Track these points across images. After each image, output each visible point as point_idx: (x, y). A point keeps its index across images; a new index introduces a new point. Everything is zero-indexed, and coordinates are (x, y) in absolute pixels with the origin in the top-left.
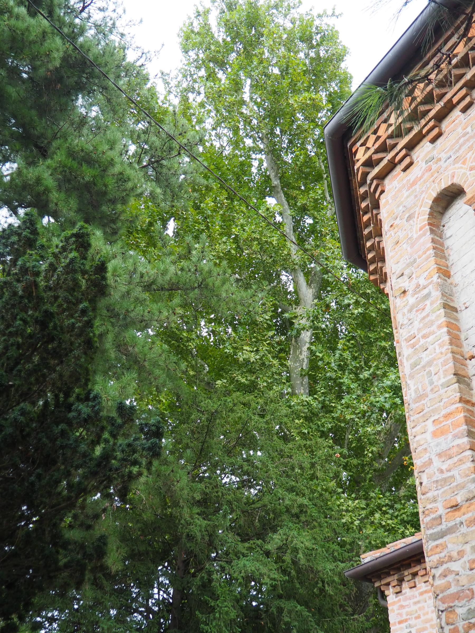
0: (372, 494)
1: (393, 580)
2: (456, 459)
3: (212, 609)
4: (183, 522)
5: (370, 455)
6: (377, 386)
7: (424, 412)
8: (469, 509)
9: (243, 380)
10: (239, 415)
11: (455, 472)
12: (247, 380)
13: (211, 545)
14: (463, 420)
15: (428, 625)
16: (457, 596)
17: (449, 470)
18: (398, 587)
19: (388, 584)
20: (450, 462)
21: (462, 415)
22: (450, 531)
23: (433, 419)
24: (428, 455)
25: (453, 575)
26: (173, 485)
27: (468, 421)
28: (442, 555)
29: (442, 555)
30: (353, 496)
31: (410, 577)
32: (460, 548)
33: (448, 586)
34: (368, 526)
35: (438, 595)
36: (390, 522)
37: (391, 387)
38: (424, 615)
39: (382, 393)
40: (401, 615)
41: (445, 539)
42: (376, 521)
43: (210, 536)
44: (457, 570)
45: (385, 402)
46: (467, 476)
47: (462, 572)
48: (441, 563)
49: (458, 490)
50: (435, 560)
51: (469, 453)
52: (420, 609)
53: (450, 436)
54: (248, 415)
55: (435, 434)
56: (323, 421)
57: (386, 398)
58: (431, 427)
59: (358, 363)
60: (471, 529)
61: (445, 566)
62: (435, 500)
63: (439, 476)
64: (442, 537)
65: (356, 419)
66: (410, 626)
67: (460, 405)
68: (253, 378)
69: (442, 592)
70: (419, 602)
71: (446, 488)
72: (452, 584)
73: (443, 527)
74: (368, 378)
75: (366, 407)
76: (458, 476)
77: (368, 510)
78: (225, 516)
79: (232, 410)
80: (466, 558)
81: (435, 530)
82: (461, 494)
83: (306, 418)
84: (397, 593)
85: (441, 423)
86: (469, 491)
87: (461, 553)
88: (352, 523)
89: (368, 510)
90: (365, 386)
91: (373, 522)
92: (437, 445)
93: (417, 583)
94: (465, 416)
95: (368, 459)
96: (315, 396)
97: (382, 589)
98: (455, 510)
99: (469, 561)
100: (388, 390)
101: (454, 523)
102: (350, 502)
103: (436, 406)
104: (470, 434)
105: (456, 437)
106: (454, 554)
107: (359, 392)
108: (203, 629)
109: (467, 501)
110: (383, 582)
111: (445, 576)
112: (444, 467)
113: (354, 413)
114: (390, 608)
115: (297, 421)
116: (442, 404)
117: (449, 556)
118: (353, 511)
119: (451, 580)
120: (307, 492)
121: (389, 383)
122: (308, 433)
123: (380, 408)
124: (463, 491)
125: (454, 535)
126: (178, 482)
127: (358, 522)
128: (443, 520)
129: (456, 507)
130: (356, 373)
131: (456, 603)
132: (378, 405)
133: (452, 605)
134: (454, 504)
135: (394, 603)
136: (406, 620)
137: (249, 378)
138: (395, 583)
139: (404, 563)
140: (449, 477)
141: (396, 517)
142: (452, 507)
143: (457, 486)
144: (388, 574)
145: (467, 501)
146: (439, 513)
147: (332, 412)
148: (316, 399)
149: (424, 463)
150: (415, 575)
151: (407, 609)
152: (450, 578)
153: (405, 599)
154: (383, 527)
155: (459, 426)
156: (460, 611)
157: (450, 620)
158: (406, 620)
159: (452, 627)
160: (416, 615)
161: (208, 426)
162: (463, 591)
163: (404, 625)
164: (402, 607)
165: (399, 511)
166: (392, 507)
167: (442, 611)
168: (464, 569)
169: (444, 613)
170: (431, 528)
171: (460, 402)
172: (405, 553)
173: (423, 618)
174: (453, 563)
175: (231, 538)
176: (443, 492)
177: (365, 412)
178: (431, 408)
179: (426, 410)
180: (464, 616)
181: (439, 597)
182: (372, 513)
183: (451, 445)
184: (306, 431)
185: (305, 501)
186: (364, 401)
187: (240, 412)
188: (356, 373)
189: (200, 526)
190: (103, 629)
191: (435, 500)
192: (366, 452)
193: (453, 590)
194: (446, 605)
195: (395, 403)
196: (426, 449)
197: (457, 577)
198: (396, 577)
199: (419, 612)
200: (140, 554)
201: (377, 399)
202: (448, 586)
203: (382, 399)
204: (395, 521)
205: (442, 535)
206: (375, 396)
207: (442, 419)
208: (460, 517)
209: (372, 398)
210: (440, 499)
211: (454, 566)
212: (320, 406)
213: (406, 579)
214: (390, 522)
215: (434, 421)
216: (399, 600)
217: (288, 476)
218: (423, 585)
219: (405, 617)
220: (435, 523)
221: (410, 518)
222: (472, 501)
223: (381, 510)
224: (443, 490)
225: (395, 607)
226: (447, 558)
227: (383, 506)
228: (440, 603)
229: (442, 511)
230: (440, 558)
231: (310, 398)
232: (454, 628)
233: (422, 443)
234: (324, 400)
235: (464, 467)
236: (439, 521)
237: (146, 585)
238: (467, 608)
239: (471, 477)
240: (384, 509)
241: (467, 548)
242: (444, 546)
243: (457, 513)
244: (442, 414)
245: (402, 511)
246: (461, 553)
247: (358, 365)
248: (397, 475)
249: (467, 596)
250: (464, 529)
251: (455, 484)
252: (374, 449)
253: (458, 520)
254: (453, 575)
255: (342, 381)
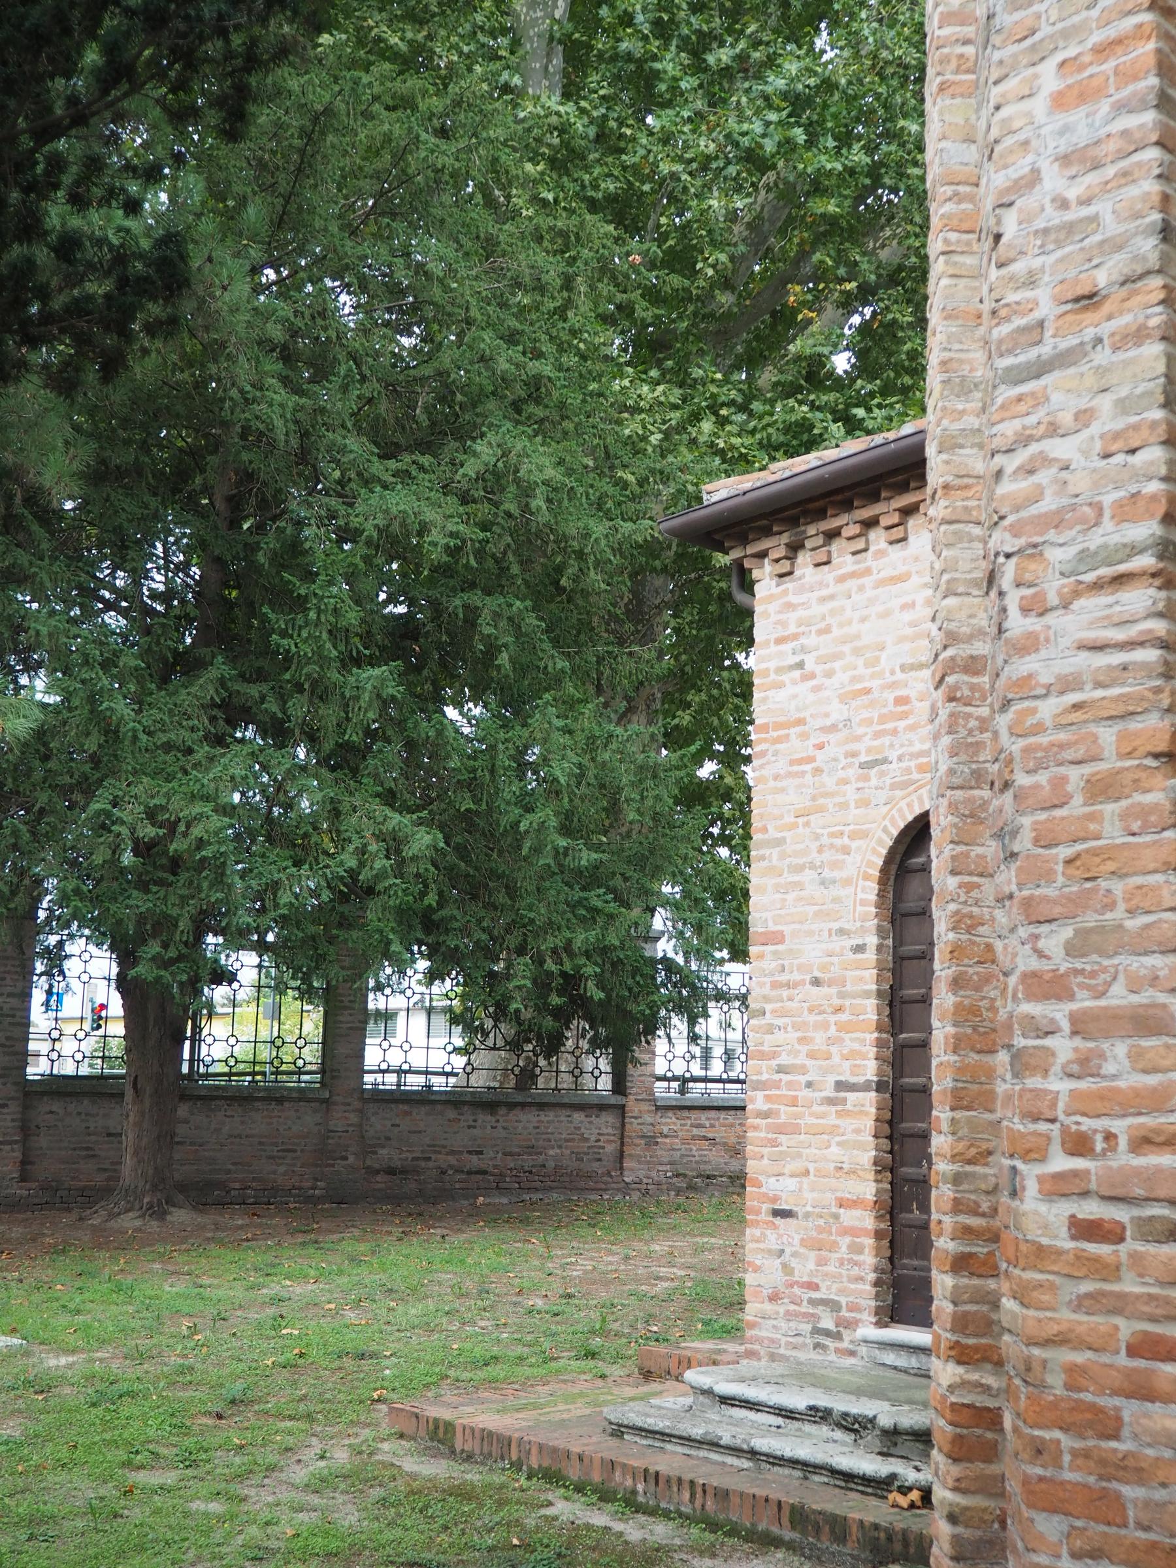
0: (697, 373)
1: (777, 545)
2: (1110, 171)
3: (301, 604)
4: (234, 393)
5: (710, 272)
6: (748, 91)
7: (1038, 36)
8: (1127, 304)
9: (394, 40)
10: (386, 127)
11: (1103, 208)
12: (402, 39)
13: (304, 458)
14: (1151, 61)
15: (846, 648)
16: (1056, 520)
17: (1086, 201)
18: (787, 563)
19: (762, 555)
20: (1093, 178)
21: (1151, 45)
22: (1063, 360)
23: (1059, 57)
24: (1030, 158)
25: (1054, 470)
26: (213, 297)
27: (1164, 68)
28: (1032, 420)
29: (1032, 420)
30: (654, 373)
31: (820, 540)
32: (1083, 403)
33: (1036, 496)
34: (683, 449)
35: (1002, 518)
36: (736, 441)
37: (785, 95)
38: (841, 626)
39: (758, 112)
40: (783, 624)
41: (1046, 380)
42: (702, 439)
43: (304, 435)
44: (1065, 456)
45: (764, 136)
46: (1138, 216)
47: (1078, 461)
48: (1025, 440)
49: (1103, 253)
50: (1010, 433)
51: (1154, 153)
52: (833, 613)
53: (1105, 107)
54: (410, 129)
55: (1059, 101)
56: (597, 171)
57: (768, 124)
58: (1049, 78)
59: (708, 22)
60: (1121, 356)
61: (1034, 448)
62: (1031, 281)
63: (1054, 217)
64: (1038, 376)
65: (685, 177)
66: (804, 650)
67: (1147, 17)
68: (420, 37)
69: (1017, 509)
70: (832, 597)
71: (1068, 249)
72: (1048, 492)
73: (1046, 350)
74: (728, 68)
75: (712, 146)
76: (1108, 218)
77: (687, 409)
78: (345, 389)
79: (368, 116)
80: (1095, 429)
81: (1022, 358)
82: (1110, 263)
83: (552, 162)
84: (781, 576)
85: (1082, 68)
86: (1135, 258)
87: (1084, 417)
88: (644, 439)
89: (687, 409)
90: (717, 87)
91: (693, 441)
92: (1062, 132)
93: (834, 555)
94: (1159, 51)
95: (702, 283)
96: (583, 104)
97: (747, 565)
98: (1086, 308)
99: (1102, 437)
100: (776, 101)
101: (1076, 341)
102: (646, 388)
103: (1076, 19)
104: (1164, 102)
105: (1122, 108)
106: (1066, 419)
107: (700, 104)
108: (278, 646)
109: (1123, 283)
110: (750, 550)
111: (1031, 472)
112: (1072, 194)
113: (680, 159)
114: (758, 609)
115: (529, 167)
116: (1095, 13)
117: (1051, 424)
118: (650, 410)
119: (1045, 482)
120: (547, 347)
121: (781, 83)
122: (556, 200)
123: (749, 151)
124: (1117, 257)
125: (1072, 370)
126: (225, 288)
127: (659, 436)
128: (1048, 334)
129: (1089, 300)
130: (698, 47)
131: (1051, 535)
132: (745, 142)
133: (1038, 539)
134: (1086, 290)
135: (770, 598)
136: (795, 637)
137: (409, 35)
138: (781, 552)
139: (811, 506)
140: (1081, 220)
141: (753, 432)
142: (1077, 300)
143: (1103, 242)
144: (767, 532)
145: (1123, 283)
146: (1037, 315)
147: (622, 151)
148: (583, 111)
149: (1016, 181)
150: (832, 535)
151: (801, 613)
152: (1044, 477)
153: (800, 591)
154: (722, 453)
155: (1136, 78)
156: (1055, 555)
157: (1028, 577)
158: (795, 637)
159: (1028, 592)
160: (822, 625)
161: (302, 152)
162: (1073, 508)
163: (787, 647)
164: (790, 606)
165: (760, 418)
166: (744, 408)
167: (1008, 556)
168: (1086, 454)
169: (1014, 560)
170: (1010, 352)
171: (1150, 8)
172: (820, 481)
173: (836, 632)
174: (1057, 441)
175: (356, 445)
176: (1061, 260)
177: (709, 158)
178: (1059, 26)
179: (1045, 30)
180: (1066, 568)
181: (1006, 522)
182: (696, 417)
183: (1103, 132)
184: (550, 197)
185: (546, 368)
186: (710, 130)
187: (390, 124)
188: (698, 47)
189: (281, 405)
190: (38, 633)
191: (1031, 281)
192: (699, 266)
193: (1048, 504)
194: (1022, 542)
195: (788, 141)
196: (1026, 143)
197: (1064, 474)
198: (785, 538)
199: (829, 620)
200: (120, 473)
201: (745, 127)
202: (1036, 496)
203: (757, 127)
204: (748, 441)
205: (1040, 369)
206: (741, 118)
207: (1087, 59)
208: (1092, 326)
209: (732, 124)
210: (1046, 278)
211: (1060, 449)
212: (592, 132)
213: (809, 544)
214: (736, 441)
215: (1063, 64)
216: (786, 592)
217: (503, 305)
218: (849, 558)
219: (792, 629)
220: (1022, 339)
221: (782, 438)
222: (1139, 284)
223: (716, 414)
224: (1059, 254)
225: (772, 608)
226: (1042, 428)
227: (723, 404)
228: (1007, 535)
229: (1046, 308)
230: (1024, 428)
231: (570, 108)
232: (1035, 595)
233: (1016, 125)
234: (605, 117)
235: (1134, 191)
236: (1035, 336)
237: (128, 552)
238: (1079, 547)
239: (1148, 220)
240: (724, 412)
241: (1105, 403)
242: (1040, 399)
243: (1089, 317)
244: (1089, 44)
245: (767, 419)
246: (1084, 417)
247: (705, 28)
248: (757, 338)
249: (1083, 520)
250: (1102, 356)
251: (1097, 238)
252: (723, 257)
253: (1089, 333)
254: (1054, 470)
255: (658, 66)
